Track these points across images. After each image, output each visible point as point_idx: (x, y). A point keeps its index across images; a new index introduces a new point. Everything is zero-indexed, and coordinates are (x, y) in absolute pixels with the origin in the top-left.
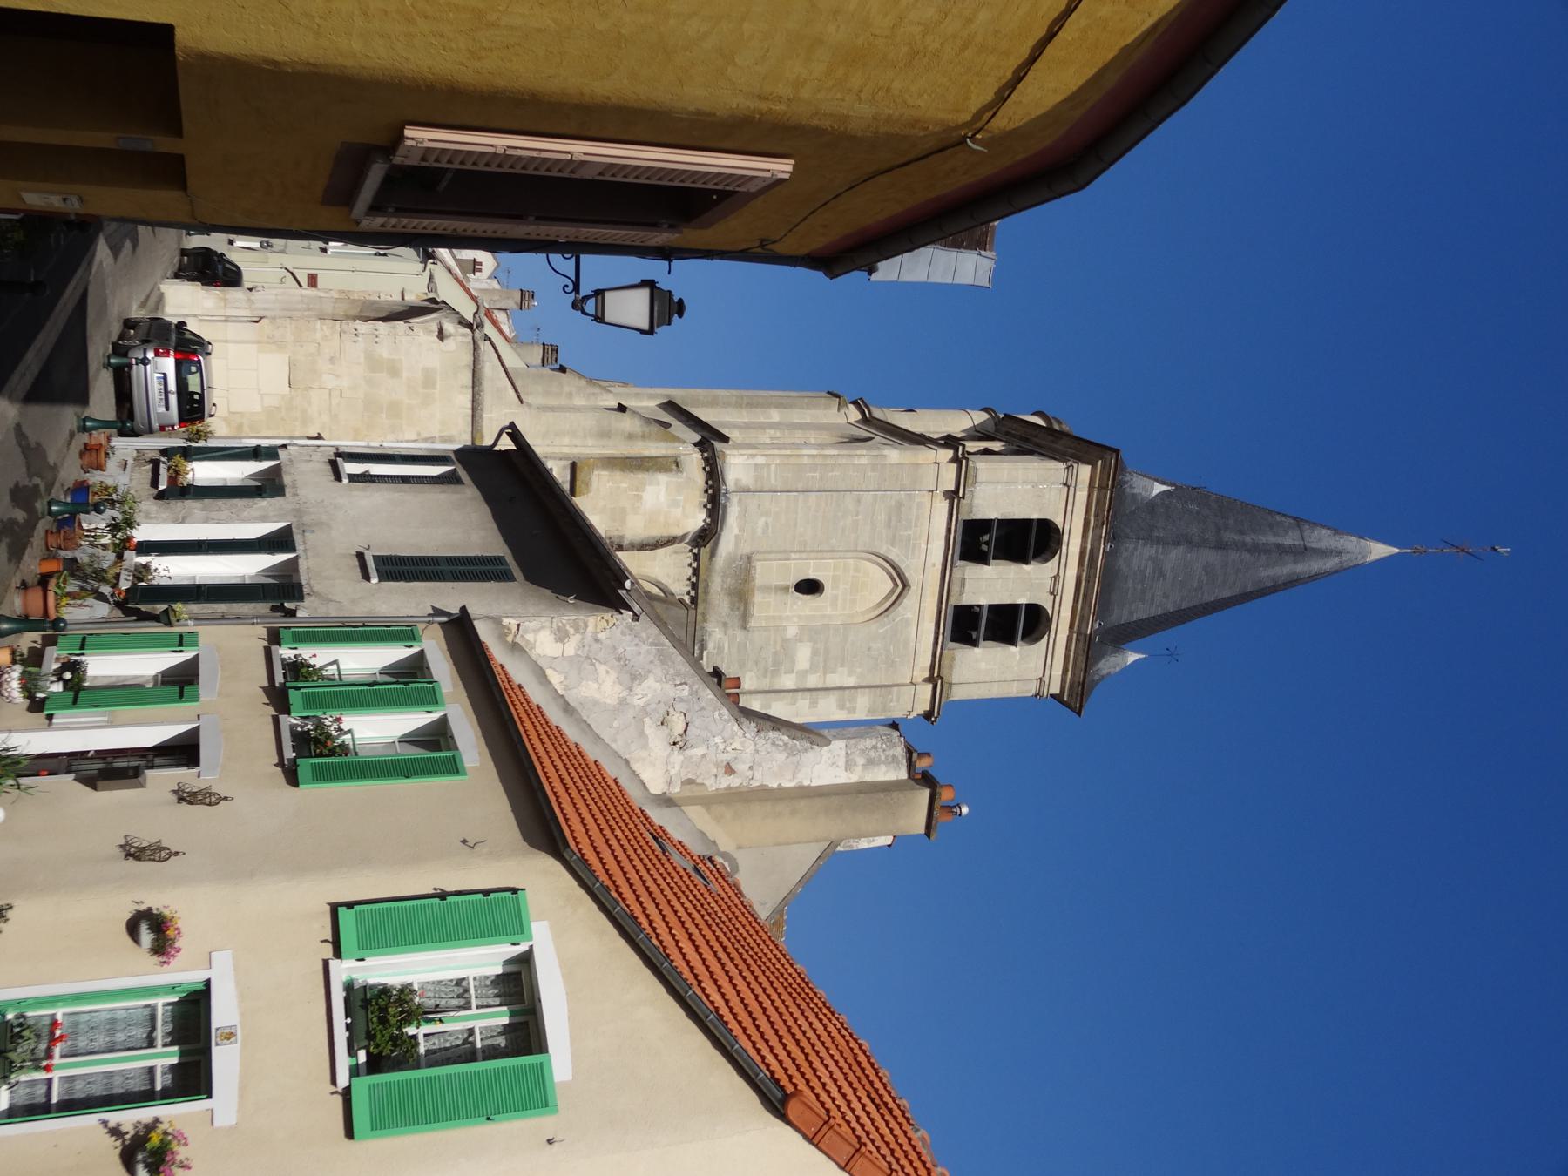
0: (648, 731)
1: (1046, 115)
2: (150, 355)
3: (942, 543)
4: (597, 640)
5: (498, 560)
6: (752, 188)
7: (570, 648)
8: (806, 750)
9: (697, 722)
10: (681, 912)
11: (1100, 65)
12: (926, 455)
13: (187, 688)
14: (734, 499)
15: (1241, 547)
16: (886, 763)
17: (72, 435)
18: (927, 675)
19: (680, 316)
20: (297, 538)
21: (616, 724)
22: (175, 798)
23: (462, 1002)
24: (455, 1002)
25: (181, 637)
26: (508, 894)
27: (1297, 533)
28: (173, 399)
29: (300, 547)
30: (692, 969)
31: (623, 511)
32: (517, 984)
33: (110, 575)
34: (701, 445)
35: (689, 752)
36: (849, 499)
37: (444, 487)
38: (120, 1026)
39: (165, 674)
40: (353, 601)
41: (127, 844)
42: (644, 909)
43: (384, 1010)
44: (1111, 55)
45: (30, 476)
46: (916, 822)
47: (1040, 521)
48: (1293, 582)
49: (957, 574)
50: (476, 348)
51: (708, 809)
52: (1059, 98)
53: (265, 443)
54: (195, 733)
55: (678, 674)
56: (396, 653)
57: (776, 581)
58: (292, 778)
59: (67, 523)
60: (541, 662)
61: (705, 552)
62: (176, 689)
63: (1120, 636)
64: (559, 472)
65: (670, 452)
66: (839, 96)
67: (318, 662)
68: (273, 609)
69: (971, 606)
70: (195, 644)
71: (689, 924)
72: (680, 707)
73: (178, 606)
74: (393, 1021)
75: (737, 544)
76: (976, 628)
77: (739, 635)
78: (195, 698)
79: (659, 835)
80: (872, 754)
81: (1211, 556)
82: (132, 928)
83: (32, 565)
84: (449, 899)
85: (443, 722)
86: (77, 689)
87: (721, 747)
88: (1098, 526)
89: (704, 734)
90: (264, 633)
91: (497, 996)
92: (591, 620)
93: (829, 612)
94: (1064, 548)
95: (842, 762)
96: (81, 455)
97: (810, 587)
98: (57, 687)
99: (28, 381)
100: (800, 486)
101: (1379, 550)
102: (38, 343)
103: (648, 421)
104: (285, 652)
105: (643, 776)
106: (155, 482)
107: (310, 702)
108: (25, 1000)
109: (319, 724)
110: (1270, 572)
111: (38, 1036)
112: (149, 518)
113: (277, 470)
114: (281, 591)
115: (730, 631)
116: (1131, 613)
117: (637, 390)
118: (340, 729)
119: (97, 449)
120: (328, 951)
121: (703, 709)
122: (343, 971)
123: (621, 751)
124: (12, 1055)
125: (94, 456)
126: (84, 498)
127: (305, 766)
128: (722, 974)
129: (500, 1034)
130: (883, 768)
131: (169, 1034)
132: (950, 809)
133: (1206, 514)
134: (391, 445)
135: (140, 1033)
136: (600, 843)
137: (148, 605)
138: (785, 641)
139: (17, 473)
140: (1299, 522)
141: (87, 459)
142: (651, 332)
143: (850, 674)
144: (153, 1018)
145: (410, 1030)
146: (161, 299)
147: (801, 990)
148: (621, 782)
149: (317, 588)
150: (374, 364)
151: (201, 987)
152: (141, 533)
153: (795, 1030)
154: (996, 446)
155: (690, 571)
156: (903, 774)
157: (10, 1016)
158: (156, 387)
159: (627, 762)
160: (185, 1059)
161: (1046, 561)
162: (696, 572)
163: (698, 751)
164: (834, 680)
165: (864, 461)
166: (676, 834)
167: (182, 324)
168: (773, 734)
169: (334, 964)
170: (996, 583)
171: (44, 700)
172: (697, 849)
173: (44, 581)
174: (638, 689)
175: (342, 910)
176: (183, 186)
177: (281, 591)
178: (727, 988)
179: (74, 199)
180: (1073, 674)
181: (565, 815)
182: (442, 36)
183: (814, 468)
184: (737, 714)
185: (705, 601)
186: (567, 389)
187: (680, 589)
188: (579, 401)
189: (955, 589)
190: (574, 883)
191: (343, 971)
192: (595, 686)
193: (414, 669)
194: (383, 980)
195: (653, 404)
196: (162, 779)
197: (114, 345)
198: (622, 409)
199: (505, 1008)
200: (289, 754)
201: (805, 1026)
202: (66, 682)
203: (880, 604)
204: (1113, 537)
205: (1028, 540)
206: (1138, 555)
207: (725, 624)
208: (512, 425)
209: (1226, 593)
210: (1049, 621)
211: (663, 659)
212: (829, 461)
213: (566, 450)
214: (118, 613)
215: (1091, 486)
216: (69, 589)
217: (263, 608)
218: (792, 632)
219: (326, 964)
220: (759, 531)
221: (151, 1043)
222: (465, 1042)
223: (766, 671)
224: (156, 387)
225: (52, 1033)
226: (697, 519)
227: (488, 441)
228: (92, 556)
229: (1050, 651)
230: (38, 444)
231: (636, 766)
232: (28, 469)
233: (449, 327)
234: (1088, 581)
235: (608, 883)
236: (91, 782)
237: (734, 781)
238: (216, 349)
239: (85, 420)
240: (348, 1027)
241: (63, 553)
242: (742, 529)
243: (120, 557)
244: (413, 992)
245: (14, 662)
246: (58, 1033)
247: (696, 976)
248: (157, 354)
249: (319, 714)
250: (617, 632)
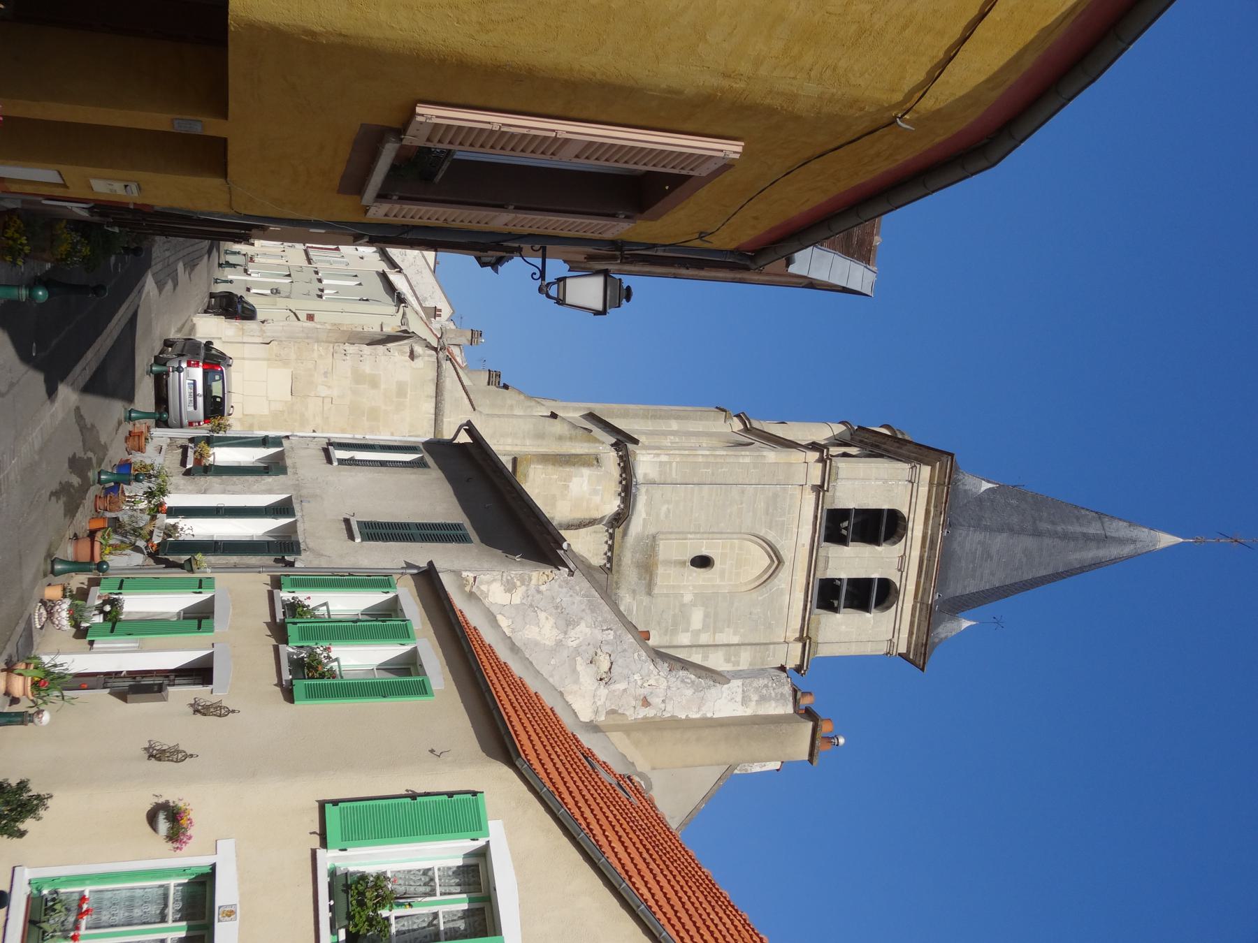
0: (579, 668)
1: (967, 96)
2: (184, 365)
3: (810, 527)
4: (539, 592)
5: (458, 527)
6: (702, 172)
7: (517, 598)
8: (709, 687)
9: (620, 662)
10: (611, 818)
11: (1021, 46)
12: (797, 456)
13: (204, 622)
14: (643, 489)
15: (1054, 535)
16: (777, 700)
17: (120, 423)
18: (797, 635)
19: (628, 299)
20: (296, 507)
21: (553, 662)
22: (191, 710)
23: (428, 889)
24: (422, 889)
25: (201, 581)
26: (469, 796)
27: (1099, 525)
28: (200, 400)
29: (298, 514)
30: (623, 866)
32: (475, 874)
33: (145, 532)
34: (617, 446)
35: (613, 687)
36: (735, 489)
37: (415, 470)
38: (138, 902)
39: (186, 611)
41: (150, 747)
42: (582, 813)
43: (362, 894)
44: (1032, 36)
45: (86, 448)
46: (800, 748)
47: (889, 510)
48: (1097, 565)
49: (822, 552)
50: (439, 366)
51: (628, 735)
52: (983, 78)
53: (272, 433)
54: (210, 657)
55: (605, 621)
56: (374, 598)
57: (675, 556)
58: (289, 695)
59: (113, 491)
60: (493, 609)
61: (619, 532)
62: (196, 622)
63: (957, 606)
64: (506, 461)
65: (592, 451)
66: (792, 74)
67: (312, 604)
68: (276, 561)
69: (834, 580)
70: (212, 586)
71: (618, 828)
72: (606, 648)
73: (199, 557)
74: (370, 904)
75: (645, 526)
76: (837, 597)
77: (646, 600)
78: (211, 630)
79: (588, 755)
80: (764, 691)
81: (1028, 542)
82: (152, 818)
83: (83, 521)
84: (419, 799)
85: (414, 653)
86: (113, 617)
87: (639, 683)
88: (937, 516)
89: (626, 671)
90: (268, 580)
91: (458, 885)
92: (535, 575)
93: (718, 582)
94: (909, 533)
95: (739, 698)
96: (127, 439)
97: (703, 562)
98: (99, 619)
99: (87, 375)
101: (1166, 540)
102: (96, 346)
103: (575, 426)
104: (285, 595)
105: (574, 706)
106: (183, 463)
107: (304, 635)
108: (59, 878)
109: (312, 653)
110: (1077, 556)
111: (68, 910)
112: (178, 489)
113: (281, 455)
114: (283, 547)
115: (638, 597)
116: (965, 587)
117: (564, 404)
118: (329, 657)
119: (140, 435)
120: (316, 841)
121: (624, 650)
122: (329, 859)
123: (557, 685)
124: (44, 925)
125: (137, 441)
126: (126, 473)
127: (300, 686)
128: (648, 871)
129: (461, 918)
130: (773, 704)
131: (179, 911)
132: (828, 739)
133: (1025, 508)
134: (371, 438)
135: (154, 910)
136: (544, 756)
137: (174, 556)
138: (683, 605)
139: (75, 447)
140: (1100, 515)
141: (130, 443)
143: (735, 633)
144: (165, 897)
145: (384, 913)
146: (193, 327)
147: (710, 889)
148: (557, 711)
149: (311, 545)
150: (358, 378)
151: (208, 870)
152: (171, 501)
153: (709, 922)
154: (853, 451)
155: (606, 547)
156: (790, 709)
157: (45, 892)
158: (187, 390)
159: (561, 694)
160: (192, 933)
161: (895, 543)
162: (611, 548)
163: (620, 686)
164: (722, 638)
165: (747, 460)
167: (209, 344)
168: (681, 673)
169: (321, 853)
170: (855, 561)
171: (87, 629)
172: (619, 769)
173: (92, 534)
174: (572, 633)
175: (328, 807)
176: (224, 173)
177: (283, 547)
178: (652, 883)
179: (134, 187)
180: (918, 637)
181: (515, 732)
182: (457, 7)
183: (707, 465)
184: (653, 656)
185: (618, 572)
186: (509, 402)
187: (598, 560)
188: (518, 412)
189: (821, 565)
190: (525, 788)
191: (329, 859)
192: (537, 629)
193: (391, 610)
194: (361, 869)
195: (577, 415)
196: (183, 694)
197: (156, 357)
198: (554, 416)
199: (464, 896)
200: (287, 676)
201: (717, 921)
202: (106, 614)
203: (760, 576)
204: (950, 525)
205: (878, 526)
206: (970, 540)
207: (634, 591)
208: (469, 423)
209: (1042, 572)
210: (898, 592)
211: (593, 608)
212: (719, 460)
213: (508, 448)
214: (151, 562)
215: (931, 483)
216: (111, 542)
217: (268, 560)
218: (688, 598)
219: (314, 853)
220: (662, 516)
221: (163, 919)
222: (430, 924)
223: (666, 631)
224: (187, 390)
225: (80, 907)
226: (612, 505)
227: (447, 435)
228: (131, 516)
229: (898, 618)
230: (93, 426)
231: (569, 698)
232: (84, 445)
233: (419, 349)
234: (929, 560)
235: (552, 789)
236: (123, 696)
237: (650, 712)
238: (235, 364)
239: (130, 412)
240: (331, 908)
241: (108, 515)
242: (648, 514)
243: (154, 518)
244: (387, 879)
245: (64, 596)
246: (85, 907)
247: (627, 872)
248: (189, 365)
249: (312, 644)
250: (555, 585)
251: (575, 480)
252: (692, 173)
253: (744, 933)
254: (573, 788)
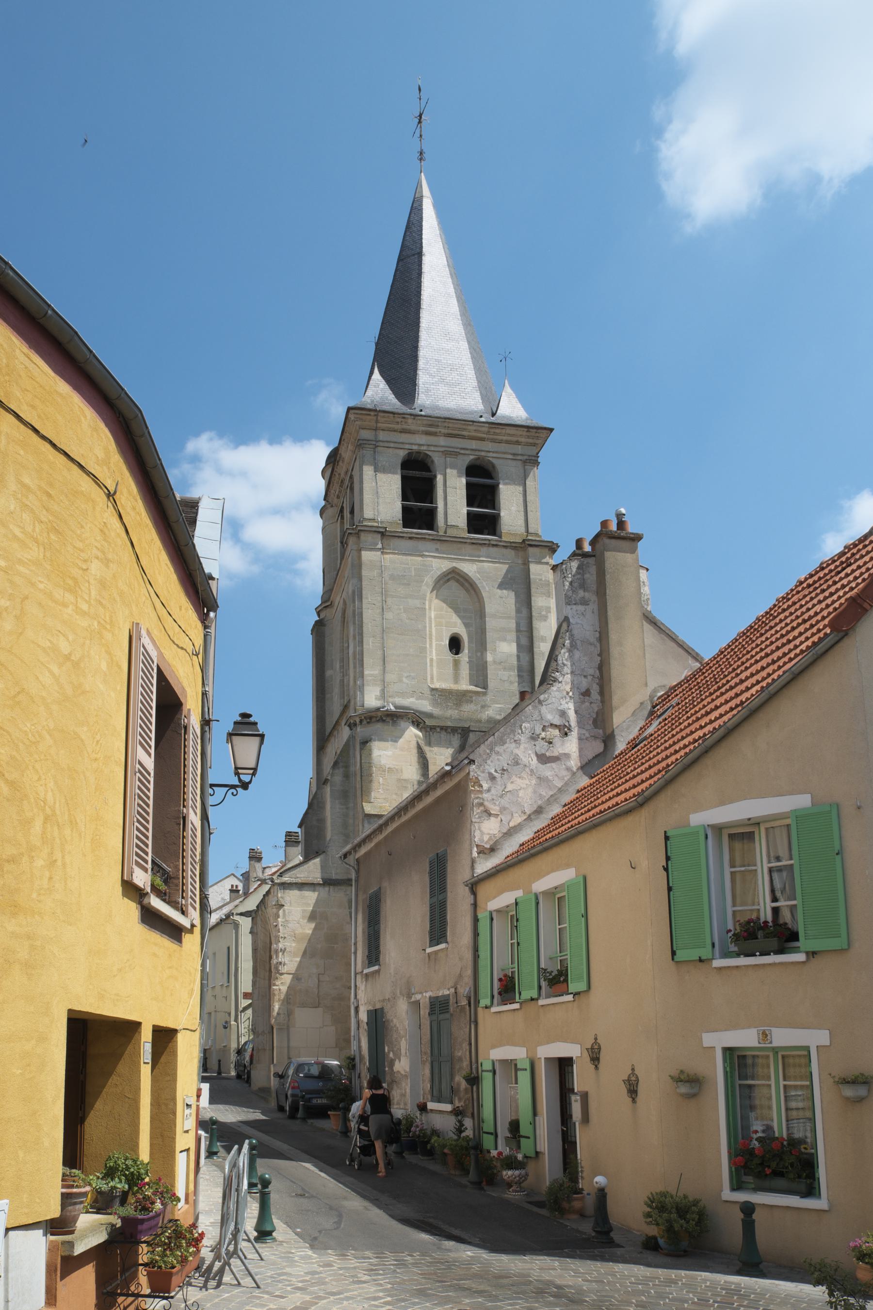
19: (249, 716)
31: (399, 780)
40: (461, 959)
100: (380, 653)
142: (262, 736)
166: (635, 732)
203: (467, 590)
207: (483, 707)
251: (383, 762)
252: (155, 664)
253: (795, 599)
254: (663, 755)
